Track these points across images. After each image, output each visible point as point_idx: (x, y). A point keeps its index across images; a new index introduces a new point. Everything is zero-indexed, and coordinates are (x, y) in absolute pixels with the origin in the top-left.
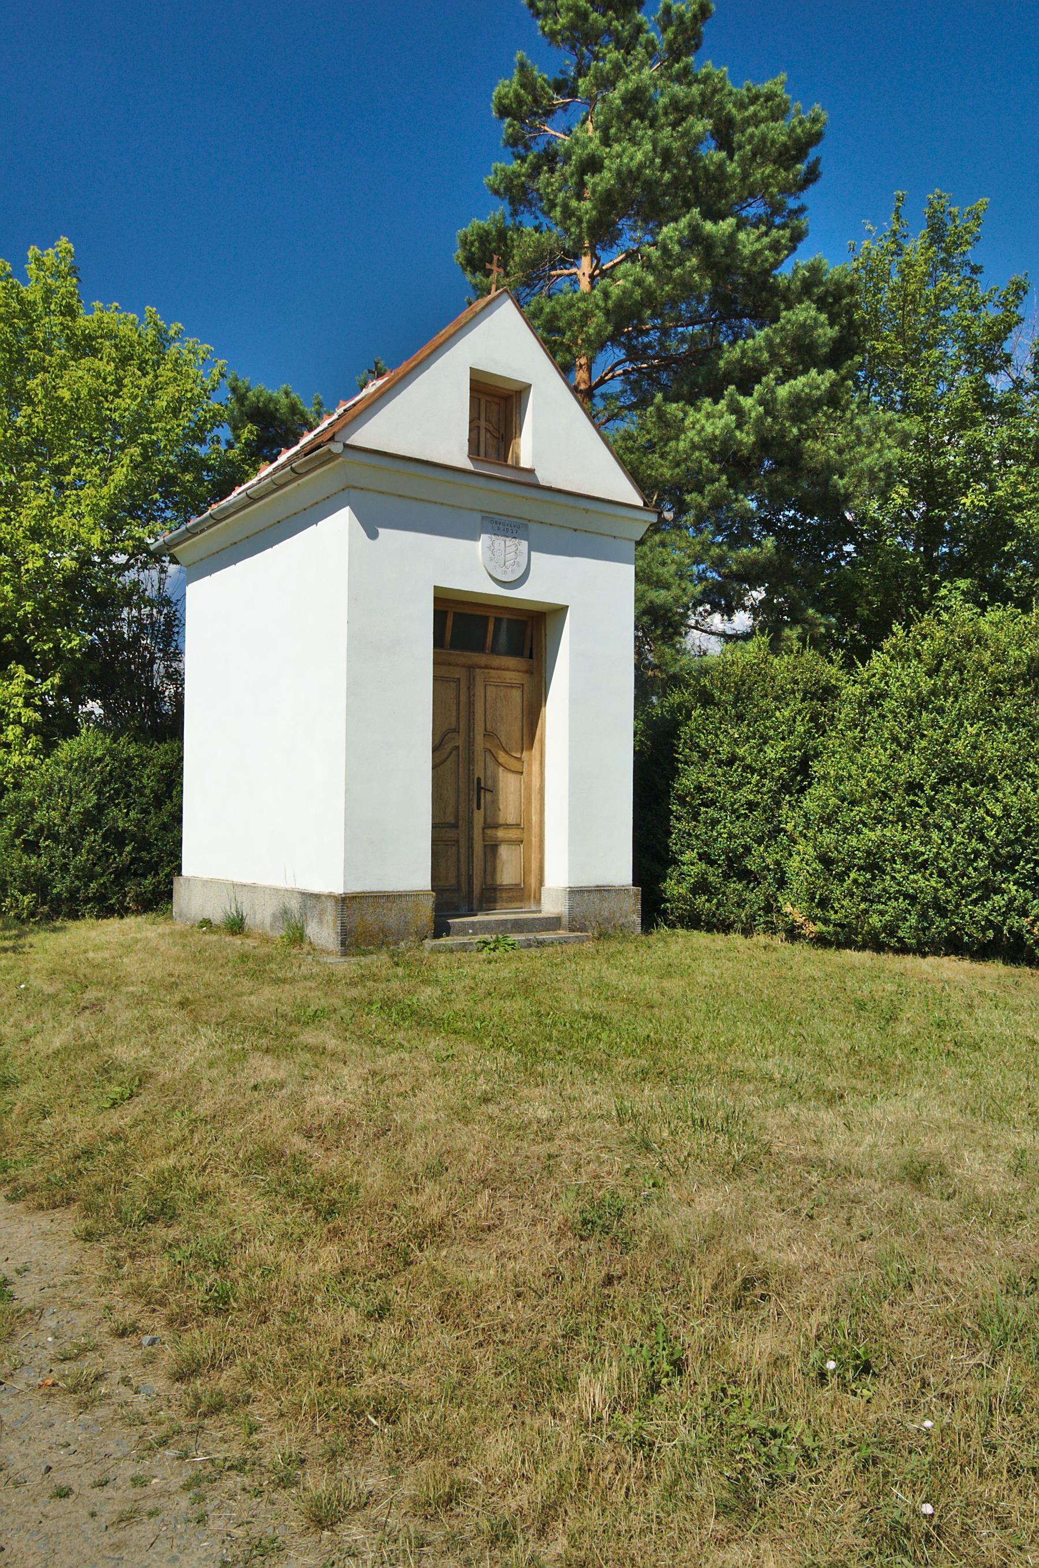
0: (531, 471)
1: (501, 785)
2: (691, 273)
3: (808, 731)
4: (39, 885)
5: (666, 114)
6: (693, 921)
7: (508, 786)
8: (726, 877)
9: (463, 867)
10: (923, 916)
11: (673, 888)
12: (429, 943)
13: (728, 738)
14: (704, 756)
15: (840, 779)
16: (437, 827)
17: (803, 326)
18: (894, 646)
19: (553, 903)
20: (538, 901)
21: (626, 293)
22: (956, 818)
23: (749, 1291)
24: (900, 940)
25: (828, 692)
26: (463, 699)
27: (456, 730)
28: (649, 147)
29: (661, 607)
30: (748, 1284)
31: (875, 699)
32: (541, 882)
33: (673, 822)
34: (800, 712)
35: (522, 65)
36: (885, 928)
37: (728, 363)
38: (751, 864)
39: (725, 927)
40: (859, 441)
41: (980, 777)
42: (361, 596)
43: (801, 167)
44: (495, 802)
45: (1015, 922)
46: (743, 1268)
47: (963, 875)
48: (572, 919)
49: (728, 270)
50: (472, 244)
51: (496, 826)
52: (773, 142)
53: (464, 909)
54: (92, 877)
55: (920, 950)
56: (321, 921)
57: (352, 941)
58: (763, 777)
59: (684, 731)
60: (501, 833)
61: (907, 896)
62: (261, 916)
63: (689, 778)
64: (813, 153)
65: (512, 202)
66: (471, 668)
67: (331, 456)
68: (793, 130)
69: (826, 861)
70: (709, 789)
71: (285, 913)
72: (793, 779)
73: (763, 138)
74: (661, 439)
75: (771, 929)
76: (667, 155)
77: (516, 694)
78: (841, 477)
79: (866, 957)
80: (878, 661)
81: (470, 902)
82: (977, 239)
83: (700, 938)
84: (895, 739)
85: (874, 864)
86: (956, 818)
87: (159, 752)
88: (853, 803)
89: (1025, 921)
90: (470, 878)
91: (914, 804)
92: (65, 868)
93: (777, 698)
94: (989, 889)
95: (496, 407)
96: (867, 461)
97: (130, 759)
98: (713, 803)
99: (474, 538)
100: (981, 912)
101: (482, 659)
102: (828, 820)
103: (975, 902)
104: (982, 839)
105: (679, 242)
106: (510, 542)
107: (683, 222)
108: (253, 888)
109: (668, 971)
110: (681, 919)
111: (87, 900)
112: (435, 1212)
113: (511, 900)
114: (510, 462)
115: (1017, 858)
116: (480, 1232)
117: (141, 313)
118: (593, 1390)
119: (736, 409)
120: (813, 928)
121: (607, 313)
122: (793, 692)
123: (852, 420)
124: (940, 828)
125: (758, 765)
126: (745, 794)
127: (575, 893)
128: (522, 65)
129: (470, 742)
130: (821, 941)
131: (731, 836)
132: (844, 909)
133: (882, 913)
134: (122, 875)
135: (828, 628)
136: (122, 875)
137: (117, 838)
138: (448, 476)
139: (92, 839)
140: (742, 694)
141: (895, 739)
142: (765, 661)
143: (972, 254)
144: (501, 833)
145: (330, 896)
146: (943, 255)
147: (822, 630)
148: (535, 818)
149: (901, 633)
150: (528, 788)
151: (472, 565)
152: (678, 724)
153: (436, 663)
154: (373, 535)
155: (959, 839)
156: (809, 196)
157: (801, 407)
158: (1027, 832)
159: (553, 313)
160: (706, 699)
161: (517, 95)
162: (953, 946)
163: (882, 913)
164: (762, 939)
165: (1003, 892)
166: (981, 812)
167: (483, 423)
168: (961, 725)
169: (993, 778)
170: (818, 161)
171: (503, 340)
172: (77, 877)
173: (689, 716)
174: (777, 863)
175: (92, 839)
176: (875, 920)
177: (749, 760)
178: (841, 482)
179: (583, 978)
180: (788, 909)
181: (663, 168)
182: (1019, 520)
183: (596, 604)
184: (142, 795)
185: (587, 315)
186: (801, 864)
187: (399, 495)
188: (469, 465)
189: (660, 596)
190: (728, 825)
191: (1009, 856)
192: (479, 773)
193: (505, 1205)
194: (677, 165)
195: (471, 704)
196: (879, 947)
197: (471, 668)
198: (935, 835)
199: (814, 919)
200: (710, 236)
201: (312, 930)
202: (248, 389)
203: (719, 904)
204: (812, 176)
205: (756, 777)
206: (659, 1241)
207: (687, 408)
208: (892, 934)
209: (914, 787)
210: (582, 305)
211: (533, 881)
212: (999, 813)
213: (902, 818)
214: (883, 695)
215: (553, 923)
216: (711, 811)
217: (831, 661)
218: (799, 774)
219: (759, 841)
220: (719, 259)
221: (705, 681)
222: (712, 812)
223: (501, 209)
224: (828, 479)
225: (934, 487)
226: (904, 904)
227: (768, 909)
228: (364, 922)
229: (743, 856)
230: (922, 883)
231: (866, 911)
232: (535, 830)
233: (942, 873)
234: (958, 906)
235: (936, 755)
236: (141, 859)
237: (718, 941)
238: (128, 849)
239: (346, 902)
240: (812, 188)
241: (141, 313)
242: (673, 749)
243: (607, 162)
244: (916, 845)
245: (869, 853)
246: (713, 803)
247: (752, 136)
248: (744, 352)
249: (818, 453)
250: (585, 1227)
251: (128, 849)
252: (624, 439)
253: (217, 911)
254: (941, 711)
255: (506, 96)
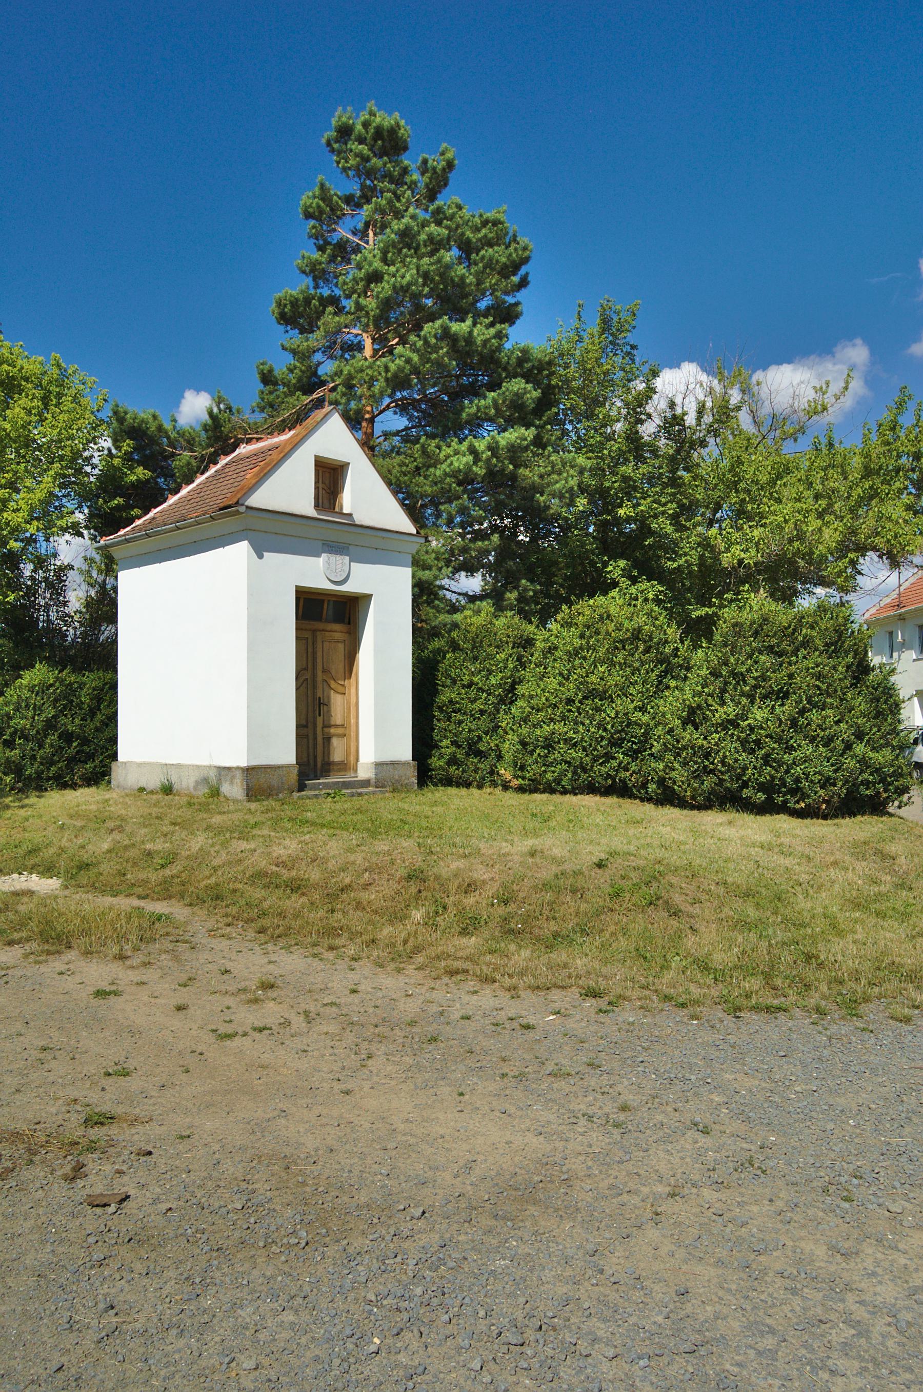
0: (350, 515)
1: (332, 701)
2: (442, 358)
3: (515, 667)
4: (16, 769)
5: (425, 246)
6: (448, 782)
7: (337, 702)
8: (468, 755)
9: (311, 750)
10: (575, 773)
11: (436, 762)
12: (296, 795)
13: (468, 671)
14: (454, 682)
15: (531, 697)
16: (299, 726)
17: (516, 394)
18: (563, 619)
19: (365, 771)
20: (356, 771)
21: (400, 369)
22: (592, 718)
23: (470, 888)
24: (563, 787)
25: (529, 643)
26: (310, 650)
27: (306, 669)
28: (415, 271)
29: (427, 582)
30: (469, 885)
31: (552, 649)
32: (357, 760)
33: (435, 722)
34: (511, 655)
35: (322, 186)
36: (555, 780)
37: (468, 415)
38: (482, 747)
39: (468, 785)
40: (553, 472)
41: (603, 695)
42: (255, 594)
43: (515, 279)
44: (329, 711)
45: (623, 774)
46: (467, 881)
47: (595, 749)
48: (377, 781)
49: (469, 354)
50: (285, 305)
51: (330, 726)
52: (497, 261)
53: (312, 776)
54: (52, 763)
55: (574, 792)
56: (232, 783)
57: (253, 793)
58: (489, 695)
59: (442, 667)
60: (332, 731)
61: (566, 762)
62: (186, 782)
63: (444, 697)
64: (523, 270)
65: (315, 279)
66: (314, 631)
67: (238, 513)
68: (510, 255)
69: (524, 744)
70: (457, 702)
71: (206, 780)
72: (506, 696)
73: (491, 259)
74: (424, 465)
75: (494, 784)
76: (426, 276)
77: (341, 646)
78: (542, 495)
79: (545, 796)
80: (553, 626)
81: (315, 772)
82: (634, 328)
83: (452, 791)
84: (561, 674)
85: (549, 745)
86: (592, 718)
87: (91, 679)
88: (538, 710)
89: (628, 774)
90: (315, 757)
91: (570, 711)
92: (33, 758)
93: (498, 647)
94: (609, 757)
95: (330, 476)
96: (558, 486)
97: (71, 684)
98: (459, 710)
99: (319, 556)
100: (604, 770)
101: (321, 625)
102: (525, 720)
103: (601, 764)
104: (605, 730)
105: (435, 336)
106: (339, 557)
107: (438, 323)
108: (179, 766)
109: (435, 804)
110: (441, 781)
111: (49, 779)
112: (347, 881)
113: (340, 770)
114: (337, 509)
115: (623, 740)
116: (366, 886)
117: (47, 356)
118: (417, 915)
119: (473, 451)
120: (515, 783)
121: (387, 380)
122: (507, 643)
123: (549, 456)
124: (583, 724)
125: (486, 688)
126: (478, 705)
127: (379, 765)
128: (322, 186)
129: (314, 676)
130: (521, 789)
131: (470, 730)
132: (533, 770)
133: (553, 772)
134: (73, 761)
135: (535, 592)
136: (73, 761)
137: (68, 737)
138: (304, 521)
139: (52, 738)
140: (476, 644)
141: (561, 674)
142: (491, 623)
143: (631, 338)
144: (332, 731)
145: (238, 768)
146: (611, 338)
147: (531, 593)
148: (353, 721)
149: (568, 611)
150: (349, 703)
151: (317, 572)
152: (438, 662)
153: (298, 629)
154: (261, 557)
155: (593, 730)
156: (521, 296)
157: (515, 452)
158: (628, 726)
159: (349, 374)
160: (455, 646)
161: (319, 206)
162: (591, 789)
163: (553, 772)
164: (489, 790)
165: (614, 758)
166: (604, 715)
167: (321, 485)
168: (596, 666)
169: (610, 696)
170: (527, 274)
171: (333, 437)
172: (41, 764)
173: (444, 657)
174: (497, 745)
175: (52, 738)
176: (549, 776)
177: (480, 685)
178: (542, 499)
179: (388, 807)
180: (502, 772)
181: (424, 285)
182: (654, 525)
183: (388, 593)
184: (81, 709)
185: (373, 379)
186: (509, 746)
187: (274, 533)
188: (311, 511)
189: (426, 575)
190: (468, 724)
191: (619, 739)
192: (319, 694)
193: (376, 876)
194: (432, 281)
195: (314, 653)
196: (553, 791)
197: (314, 631)
198: (581, 728)
199: (516, 777)
200: (455, 334)
201: (226, 789)
202: (126, 413)
203: (464, 771)
204: (524, 283)
205: (485, 695)
206: (437, 878)
207: (441, 443)
208: (559, 784)
209: (570, 701)
210: (370, 372)
211: (352, 759)
212: (613, 715)
213: (564, 718)
214: (556, 648)
215: (366, 783)
216: (458, 715)
217: (531, 622)
218: (509, 694)
219: (486, 733)
220: (461, 348)
221: (454, 635)
222: (459, 716)
223: (308, 281)
224: (534, 496)
225: (603, 500)
226: (565, 767)
227: (492, 773)
228: (259, 782)
229: (477, 742)
230: (574, 754)
231: (545, 771)
232: (353, 728)
233: (584, 749)
234: (592, 766)
235: (581, 683)
236: (83, 751)
237: (464, 791)
238: (75, 744)
239: (249, 771)
240: (524, 291)
241: (47, 356)
242: (435, 677)
243: (386, 277)
244: (571, 734)
245: (546, 739)
246: (459, 710)
247: (483, 257)
248: (479, 409)
249: (528, 477)
250: (409, 877)
251: (75, 744)
252: (400, 466)
253: (153, 781)
254: (585, 658)
255: (310, 206)
